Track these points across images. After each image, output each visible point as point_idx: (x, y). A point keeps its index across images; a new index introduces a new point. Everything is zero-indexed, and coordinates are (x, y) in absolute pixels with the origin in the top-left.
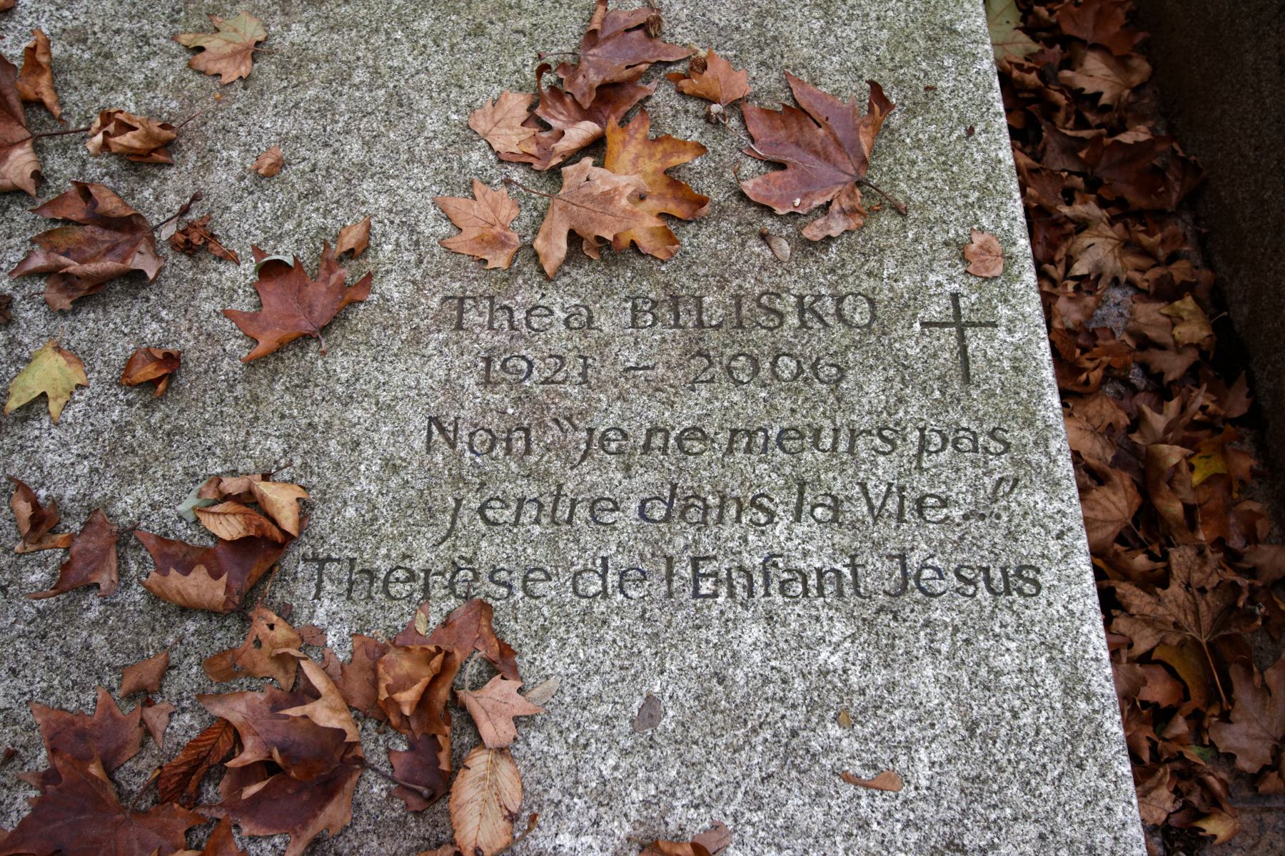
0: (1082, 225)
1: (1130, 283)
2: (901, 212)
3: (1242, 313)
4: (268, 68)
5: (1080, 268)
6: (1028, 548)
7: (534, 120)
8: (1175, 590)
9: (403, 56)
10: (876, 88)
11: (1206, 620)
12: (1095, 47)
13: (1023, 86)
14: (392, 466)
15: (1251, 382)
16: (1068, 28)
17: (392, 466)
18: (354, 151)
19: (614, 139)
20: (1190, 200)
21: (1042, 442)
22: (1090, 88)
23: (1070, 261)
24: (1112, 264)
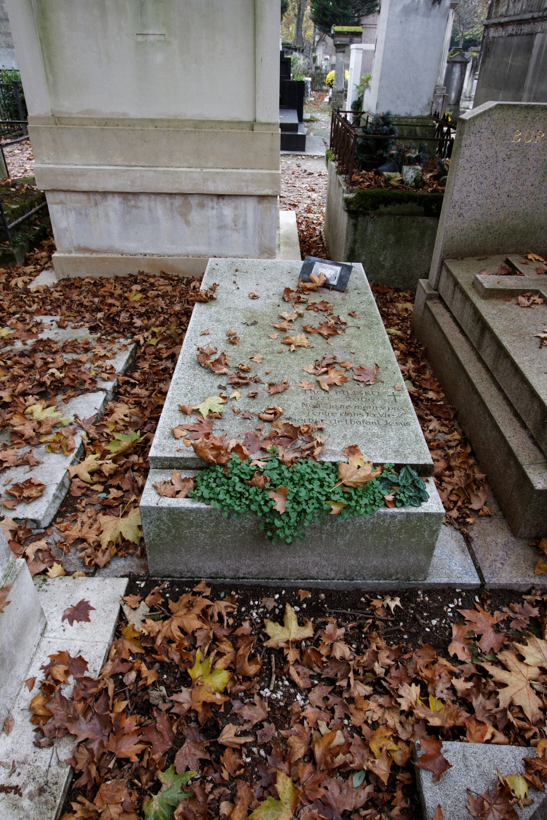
0: (430, 421)
1: (443, 432)
2: (383, 382)
3: (468, 434)
4: (265, 361)
5: (430, 428)
6: (408, 421)
7: (315, 368)
8: (455, 477)
9: (289, 360)
10: (376, 365)
11: (463, 482)
12: (430, 390)
13: (415, 397)
14: (296, 408)
15: (471, 445)
16: (424, 386)
17: (296, 408)
18: (282, 372)
19: (330, 371)
20: (456, 417)
21: (410, 409)
22: (430, 397)
23: (428, 427)
24: (438, 427)
